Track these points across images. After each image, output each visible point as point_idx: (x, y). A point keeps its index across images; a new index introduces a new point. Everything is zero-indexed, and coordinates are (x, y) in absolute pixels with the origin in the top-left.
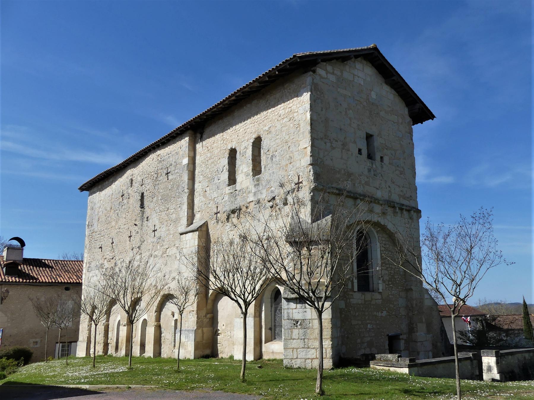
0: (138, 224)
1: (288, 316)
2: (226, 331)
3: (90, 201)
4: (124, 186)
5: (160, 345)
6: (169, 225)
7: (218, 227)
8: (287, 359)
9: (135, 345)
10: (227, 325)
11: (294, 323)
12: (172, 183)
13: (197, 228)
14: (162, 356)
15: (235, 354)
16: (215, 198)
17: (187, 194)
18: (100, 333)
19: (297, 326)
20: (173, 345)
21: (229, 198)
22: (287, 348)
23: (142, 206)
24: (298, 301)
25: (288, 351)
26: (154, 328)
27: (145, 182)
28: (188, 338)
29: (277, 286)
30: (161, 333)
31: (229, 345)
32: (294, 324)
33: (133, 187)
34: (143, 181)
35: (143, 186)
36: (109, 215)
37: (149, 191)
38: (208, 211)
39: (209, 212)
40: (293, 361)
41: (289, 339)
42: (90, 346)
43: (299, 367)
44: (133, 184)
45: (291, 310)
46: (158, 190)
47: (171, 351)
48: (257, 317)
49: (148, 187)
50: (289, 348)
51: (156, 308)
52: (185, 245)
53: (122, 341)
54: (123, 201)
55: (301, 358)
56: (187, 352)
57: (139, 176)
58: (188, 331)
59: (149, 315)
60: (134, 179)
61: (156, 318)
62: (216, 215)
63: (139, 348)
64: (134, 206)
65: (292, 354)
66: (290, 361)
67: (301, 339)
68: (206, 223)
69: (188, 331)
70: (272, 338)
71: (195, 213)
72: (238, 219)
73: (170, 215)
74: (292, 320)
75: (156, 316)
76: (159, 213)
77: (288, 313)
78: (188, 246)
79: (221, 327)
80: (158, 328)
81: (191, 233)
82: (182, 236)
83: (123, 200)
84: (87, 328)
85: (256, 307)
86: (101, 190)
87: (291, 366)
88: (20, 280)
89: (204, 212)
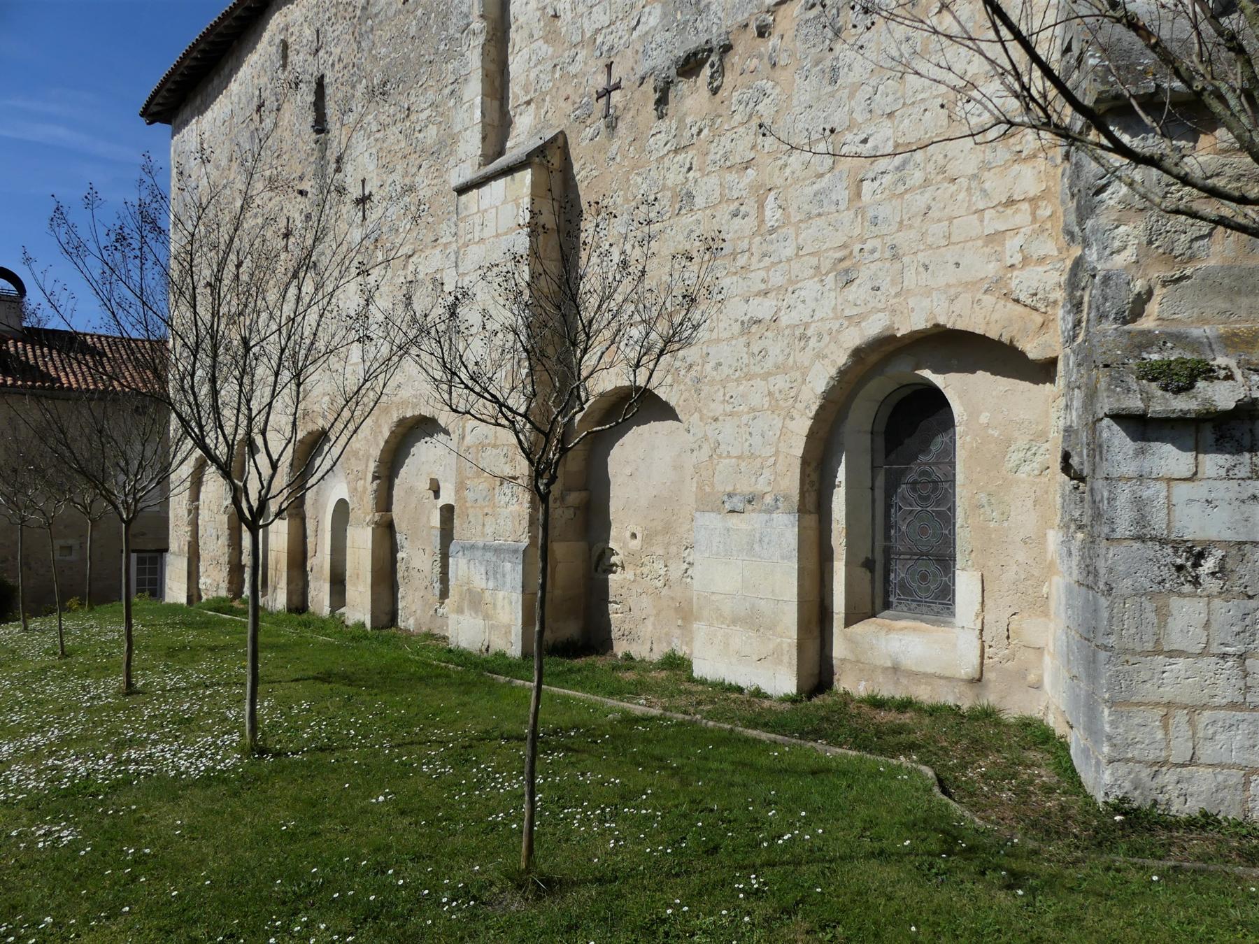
0: (309, 190)
1: (1142, 519)
2: (645, 560)
3: (175, 152)
4: (262, 73)
5: (393, 587)
6: (414, 170)
7: (615, 147)
8: (1128, 761)
9: (317, 579)
10: (648, 538)
11: (1179, 561)
12: (419, 12)
13: (529, 155)
14: (401, 624)
15: (696, 654)
16: (598, 31)
17: (481, 39)
18: (220, 533)
19: (1196, 582)
20: (437, 592)
21: (665, 15)
22: (1126, 703)
23: (320, 126)
24: (1208, 434)
25: (1137, 720)
26: (370, 530)
27: (325, 37)
28: (495, 578)
29: (927, 373)
30: (394, 549)
31: (658, 614)
32: (1180, 568)
33: (289, 68)
34: (321, 36)
35: (321, 53)
36: (225, 181)
37: (341, 65)
38: (569, 90)
39: (572, 97)
40: (1168, 777)
41: (1146, 654)
42: (198, 567)
43: (1205, 814)
44: (289, 60)
45: (1162, 486)
46: (370, 50)
47: (432, 612)
48: (810, 513)
49: (337, 51)
50: (1139, 704)
51: (377, 467)
52: (478, 228)
53: (277, 563)
54: (263, 125)
55: (1221, 765)
56: (492, 627)
57: (306, 25)
58: (497, 550)
59: (356, 489)
60: (290, 41)
61: (376, 498)
62: (603, 101)
63: (327, 587)
64: (296, 132)
65: (1160, 735)
66: (1145, 773)
67: (1224, 656)
68: (560, 141)
69: (496, 550)
70: (873, 603)
71: (512, 113)
72: (715, 91)
73: (417, 134)
74: (1163, 542)
75: (375, 491)
76: (378, 135)
77: (1140, 504)
78: (489, 232)
79: (619, 540)
80: (386, 533)
81: (501, 182)
82: (464, 198)
83: (261, 123)
84: (186, 518)
85: (809, 470)
86: (201, 111)
87: (1155, 803)
88: (6, 381)
89: (552, 101)
